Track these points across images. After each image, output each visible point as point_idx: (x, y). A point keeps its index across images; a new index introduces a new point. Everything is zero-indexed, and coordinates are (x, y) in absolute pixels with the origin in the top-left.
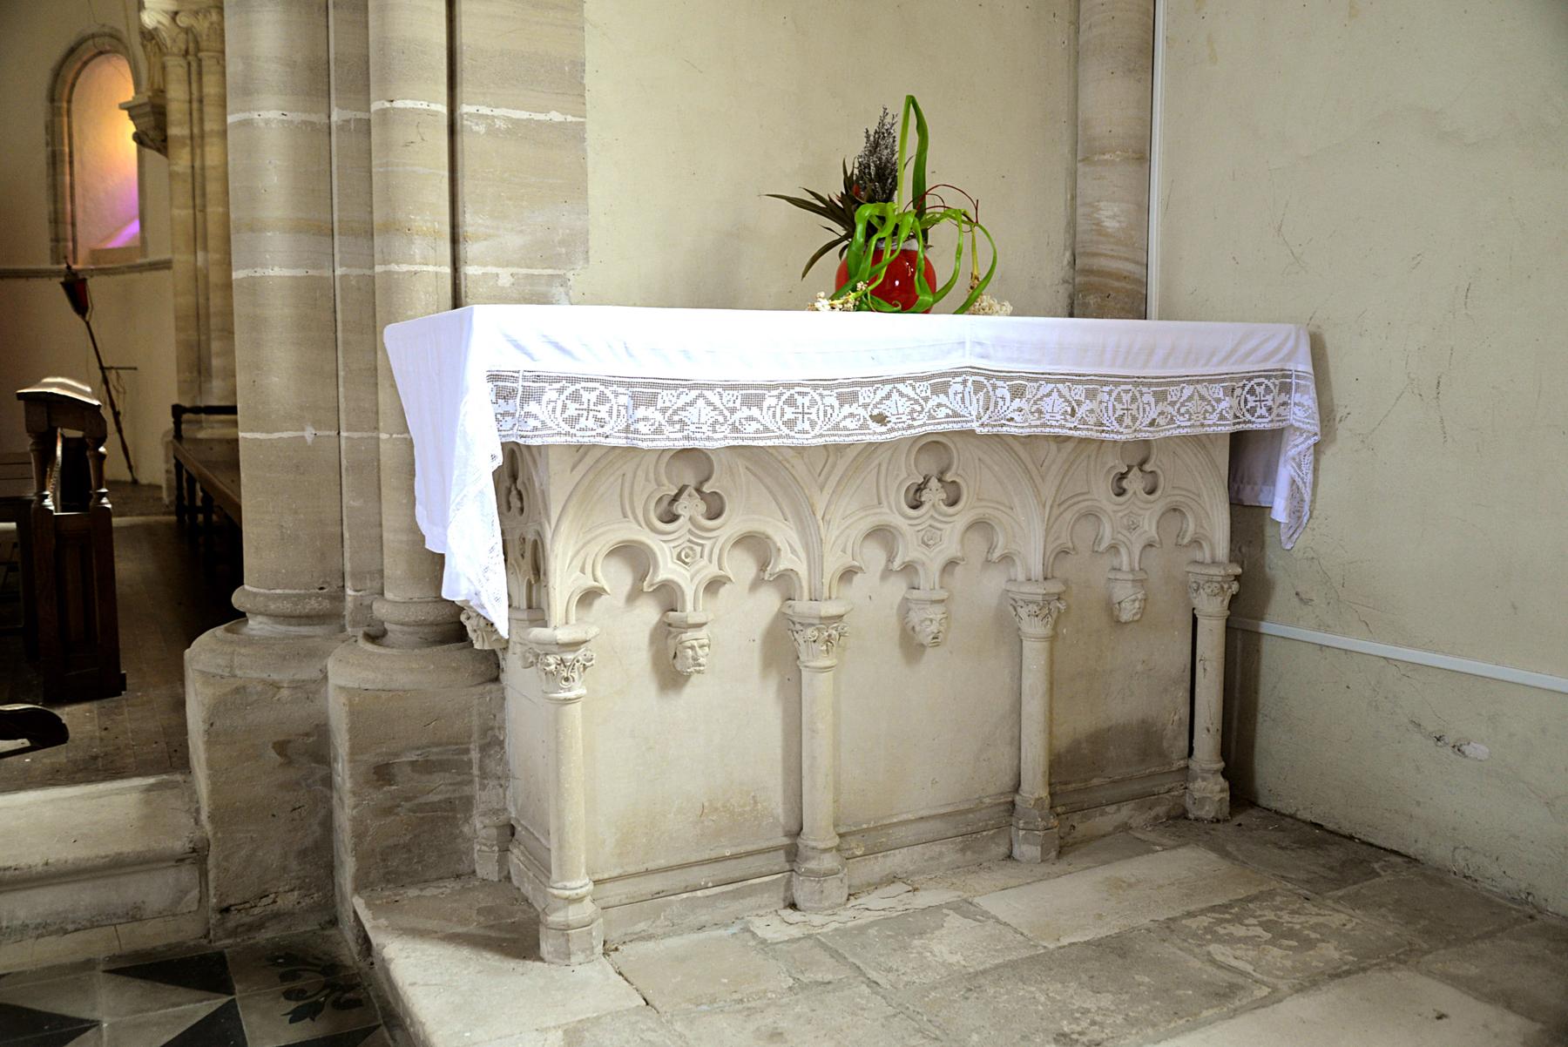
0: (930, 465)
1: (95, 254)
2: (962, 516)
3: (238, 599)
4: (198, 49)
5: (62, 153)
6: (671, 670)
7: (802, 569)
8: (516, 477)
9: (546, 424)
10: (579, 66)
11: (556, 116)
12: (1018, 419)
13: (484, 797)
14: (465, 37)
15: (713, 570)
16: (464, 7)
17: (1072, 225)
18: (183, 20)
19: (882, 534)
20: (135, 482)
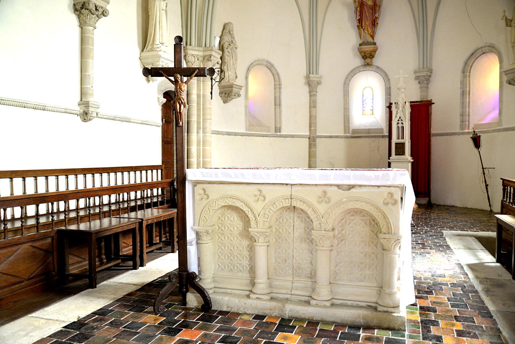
5: (466, 91)
16: (300, 2)
20: (491, 211)
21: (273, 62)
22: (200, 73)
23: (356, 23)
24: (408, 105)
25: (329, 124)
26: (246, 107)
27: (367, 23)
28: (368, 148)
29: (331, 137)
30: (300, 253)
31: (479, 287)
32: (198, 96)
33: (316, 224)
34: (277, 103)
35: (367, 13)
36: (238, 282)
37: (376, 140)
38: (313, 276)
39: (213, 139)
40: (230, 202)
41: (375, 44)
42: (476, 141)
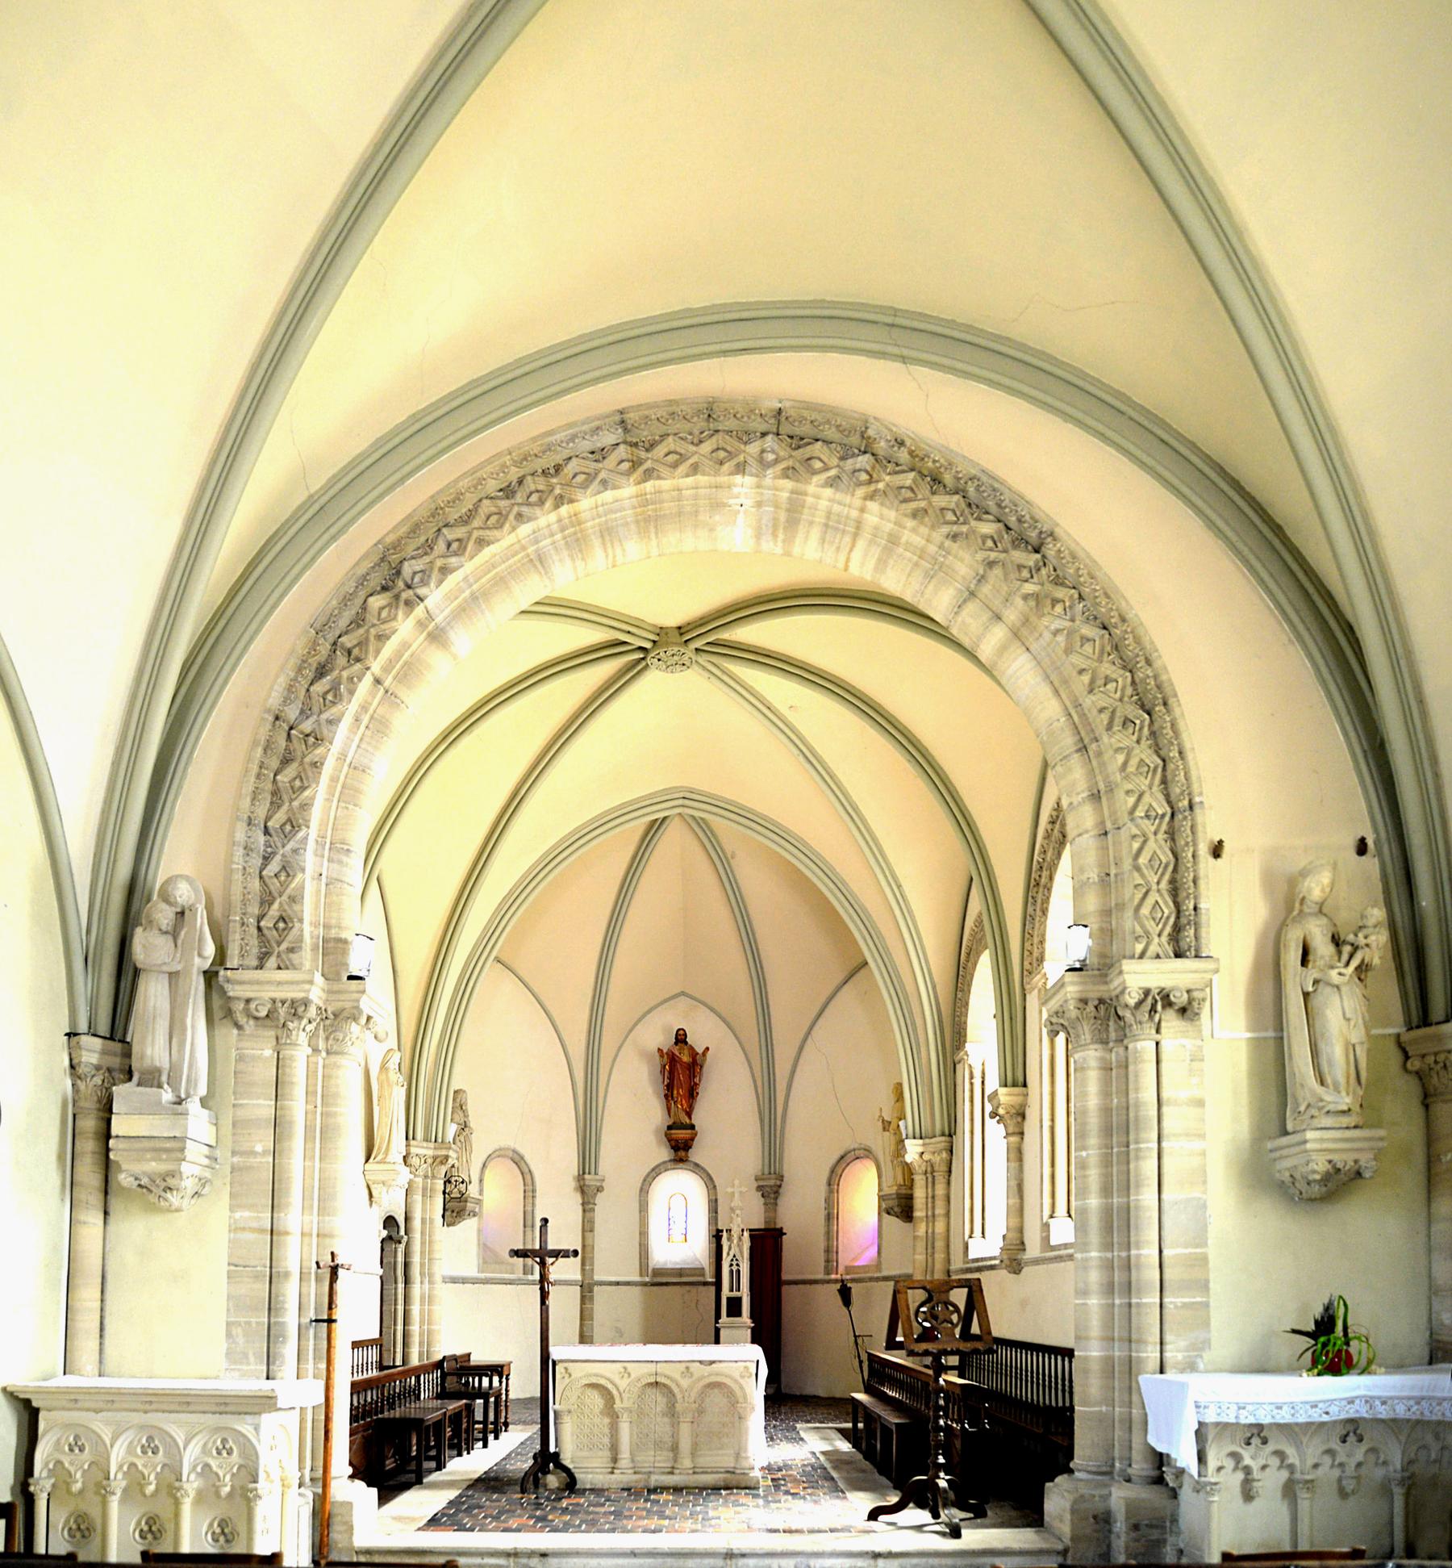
0: (1350, 1428)
1: (848, 1270)
2: (1364, 1447)
3: (1072, 1465)
4: (933, 1171)
6: (1248, 1495)
7: (1297, 1463)
8: (1201, 1434)
9: (1210, 1417)
10: (1207, 1281)
11: (1199, 1299)
12: (1383, 1412)
13: (1171, 1539)
14: (1166, 1276)
15: (1263, 1462)
17: (1430, 1320)
18: (926, 1157)
19: (1330, 1452)
21: (522, 1151)
22: (565, 1254)
23: (662, 1091)
24: (746, 1234)
25: (614, 1261)
26: (479, 1231)
27: (680, 1092)
28: (680, 1303)
29: (618, 1284)
30: (662, 1427)
31: (828, 1465)
32: (423, 1221)
33: (679, 1396)
36: (601, 1460)
37: (693, 1289)
38: (675, 1448)
39: (443, 1291)
40: (594, 1380)
41: (692, 1127)
42: (845, 1294)
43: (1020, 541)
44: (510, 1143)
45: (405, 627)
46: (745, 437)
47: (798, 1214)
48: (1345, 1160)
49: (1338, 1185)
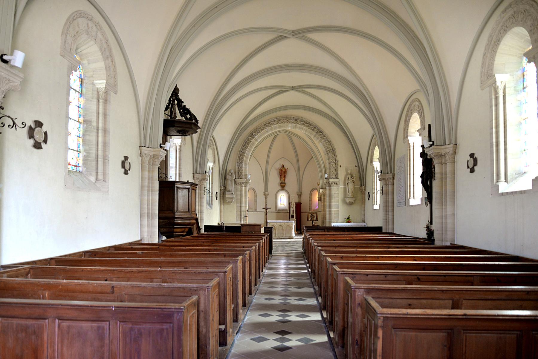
27: (283, 176)
34: (255, 201)
35: (283, 174)
43: (320, 132)
44: (252, 187)
45: (253, 140)
46: (290, 119)
47: (304, 200)
48: (351, 201)
49: (351, 204)
